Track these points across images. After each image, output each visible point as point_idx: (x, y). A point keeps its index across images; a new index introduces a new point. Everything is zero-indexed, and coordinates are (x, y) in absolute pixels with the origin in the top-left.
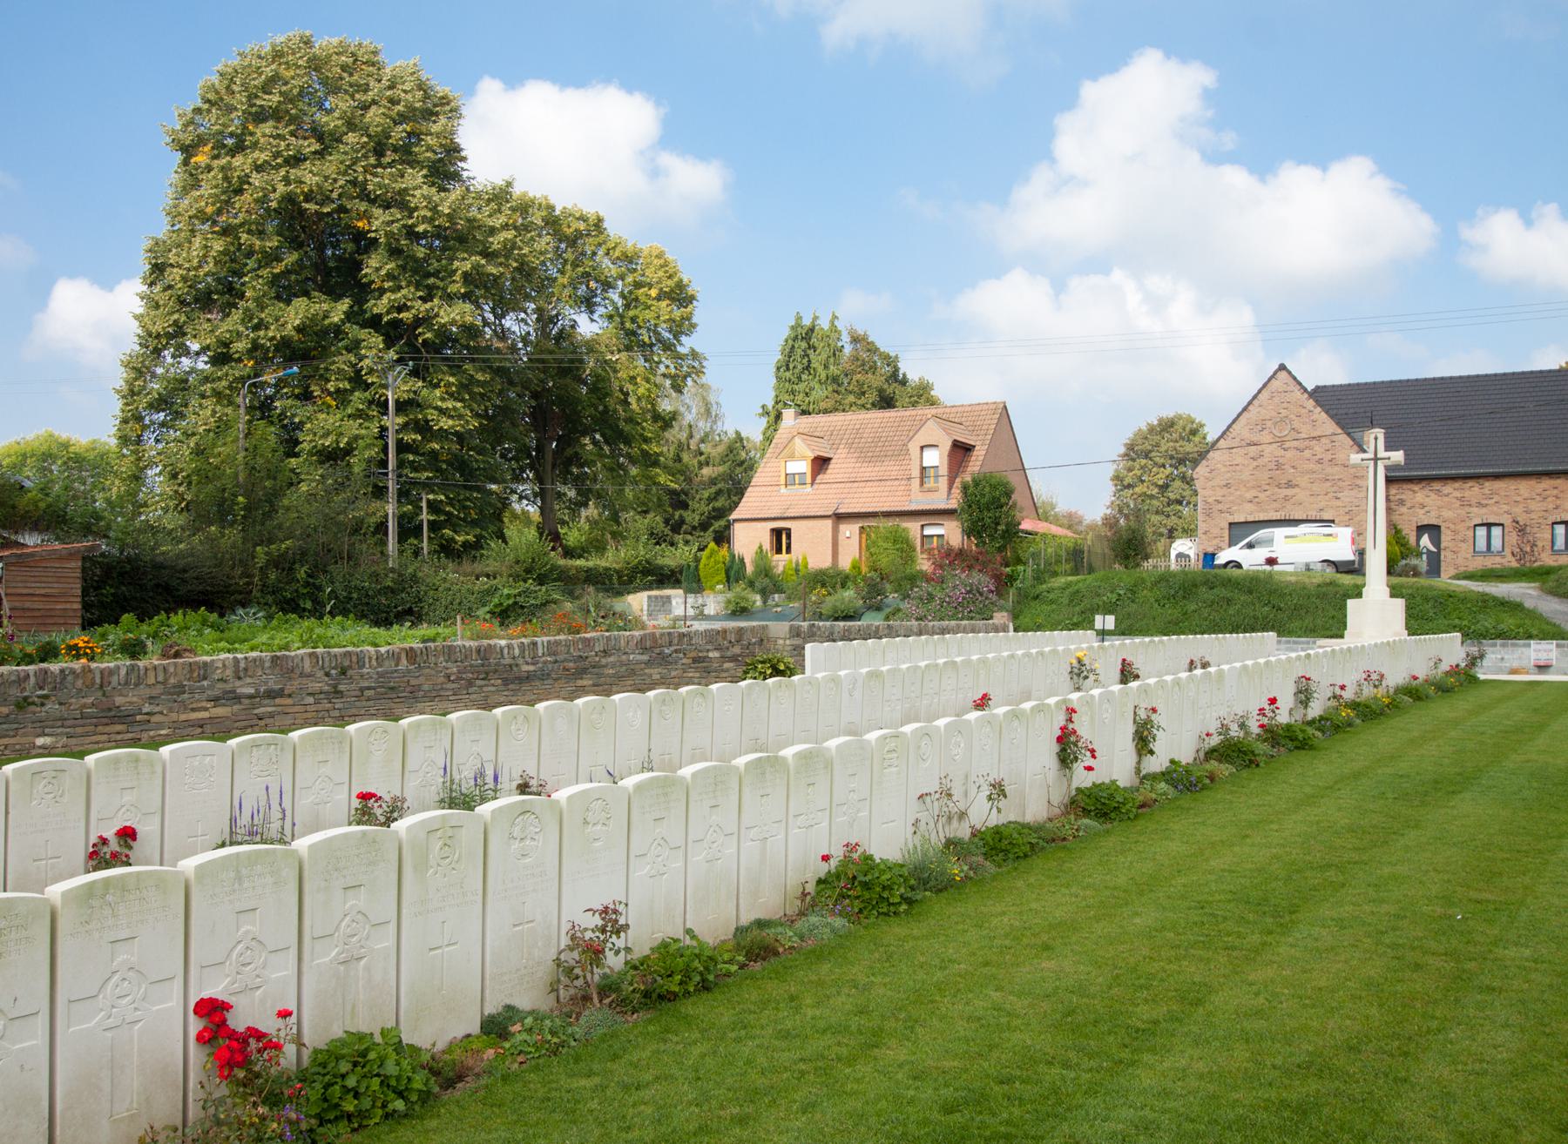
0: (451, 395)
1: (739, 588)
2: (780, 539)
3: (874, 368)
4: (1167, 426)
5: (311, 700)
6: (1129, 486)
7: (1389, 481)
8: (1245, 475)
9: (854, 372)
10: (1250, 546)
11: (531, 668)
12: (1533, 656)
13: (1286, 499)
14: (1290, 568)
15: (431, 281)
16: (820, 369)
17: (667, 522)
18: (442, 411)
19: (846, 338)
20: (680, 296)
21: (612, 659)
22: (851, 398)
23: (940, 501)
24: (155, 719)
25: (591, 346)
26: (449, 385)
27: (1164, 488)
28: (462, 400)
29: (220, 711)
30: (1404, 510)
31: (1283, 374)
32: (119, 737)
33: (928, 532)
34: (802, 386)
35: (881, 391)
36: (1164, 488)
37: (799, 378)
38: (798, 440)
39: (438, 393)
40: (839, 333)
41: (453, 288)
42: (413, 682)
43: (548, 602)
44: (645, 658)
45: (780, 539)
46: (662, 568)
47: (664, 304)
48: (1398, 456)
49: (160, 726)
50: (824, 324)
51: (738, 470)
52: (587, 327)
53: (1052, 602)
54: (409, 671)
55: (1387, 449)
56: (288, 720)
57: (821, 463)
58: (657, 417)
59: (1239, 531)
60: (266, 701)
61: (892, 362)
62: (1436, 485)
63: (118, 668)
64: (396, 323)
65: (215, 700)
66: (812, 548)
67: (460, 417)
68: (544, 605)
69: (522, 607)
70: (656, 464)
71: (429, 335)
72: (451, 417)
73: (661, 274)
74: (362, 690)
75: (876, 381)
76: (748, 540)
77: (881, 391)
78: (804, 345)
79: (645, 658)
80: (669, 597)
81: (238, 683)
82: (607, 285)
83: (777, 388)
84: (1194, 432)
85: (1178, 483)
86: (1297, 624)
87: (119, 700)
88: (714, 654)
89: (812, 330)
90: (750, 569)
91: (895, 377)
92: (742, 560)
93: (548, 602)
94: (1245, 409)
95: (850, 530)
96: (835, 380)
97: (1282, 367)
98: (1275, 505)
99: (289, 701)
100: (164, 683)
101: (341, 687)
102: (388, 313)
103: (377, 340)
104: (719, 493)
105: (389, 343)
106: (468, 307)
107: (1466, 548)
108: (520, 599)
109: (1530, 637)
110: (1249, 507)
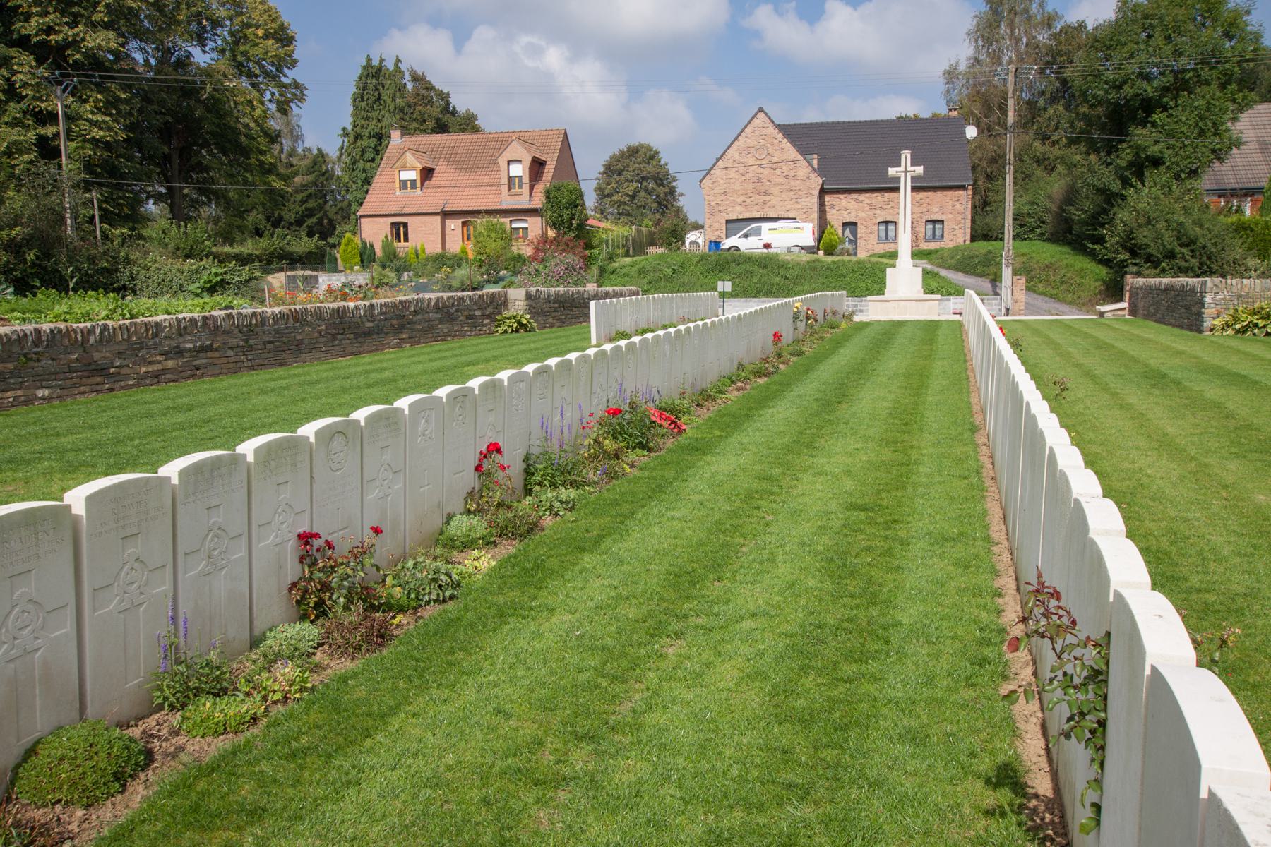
0: (99, 109)
1: (376, 267)
2: (400, 231)
3: (431, 103)
4: (633, 152)
5: (230, 353)
6: (609, 196)
7: (914, 189)
8: (737, 187)
9: (416, 105)
10: (746, 236)
11: (371, 325)
12: (952, 307)
13: (764, 203)
14: (778, 251)
15: (75, 9)
16: (389, 101)
17: (268, 219)
18: (94, 124)
19: (407, 76)
20: (283, 37)
21: (419, 317)
22: (415, 125)
23: (523, 201)
24: (124, 371)
25: (208, 72)
26: (98, 100)
27: (633, 197)
28: (110, 115)
29: (171, 363)
30: (834, 211)
31: (761, 115)
32: (99, 388)
33: (514, 226)
34: (375, 114)
35: (438, 120)
36: (633, 197)
37: (372, 108)
38: (408, 154)
39: (88, 107)
40: (403, 73)
41: (96, 17)
42: (299, 337)
43: (251, 279)
44: (439, 316)
45: (400, 231)
46: (292, 254)
47: (271, 42)
48: (919, 170)
49: (127, 377)
50: (390, 65)
51: (322, 179)
52: (201, 58)
53: (625, 275)
54: (295, 328)
55: (899, 166)
56: (522, 357)
57: (427, 173)
58: (266, 133)
59: (734, 225)
60: (201, 355)
61: (445, 97)
62: (855, 196)
63: (93, 327)
64: (44, 43)
65: (165, 354)
66: (425, 237)
67: (110, 129)
68: (247, 281)
69: (229, 283)
70: (269, 172)
71: (78, 56)
72: (101, 129)
73: (265, 17)
74: (264, 343)
75: (435, 111)
76: (374, 232)
77: (438, 120)
78: (374, 81)
79: (439, 316)
80: (316, 278)
81: (181, 340)
82: (216, 23)
83: (353, 115)
84: (652, 157)
85: (642, 194)
86: (800, 288)
87: (97, 356)
88: (478, 313)
89: (380, 69)
90: (379, 252)
91: (448, 110)
92: (372, 246)
93: (251, 279)
94: (736, 139)
95: (454, 225)
96: (401, 110)
97: (761, 110)
98: (757, 207)
99: (216, 354)
100: (128, 340)
101: (251, 342)
102: (37, 35)
103: (30, 59)
104: (310, 196)
105: (40, 61)
106: (111, 34)
107: (873, 238)
108: (228, 277)
109: (950, 294)
110: (739, 209)
